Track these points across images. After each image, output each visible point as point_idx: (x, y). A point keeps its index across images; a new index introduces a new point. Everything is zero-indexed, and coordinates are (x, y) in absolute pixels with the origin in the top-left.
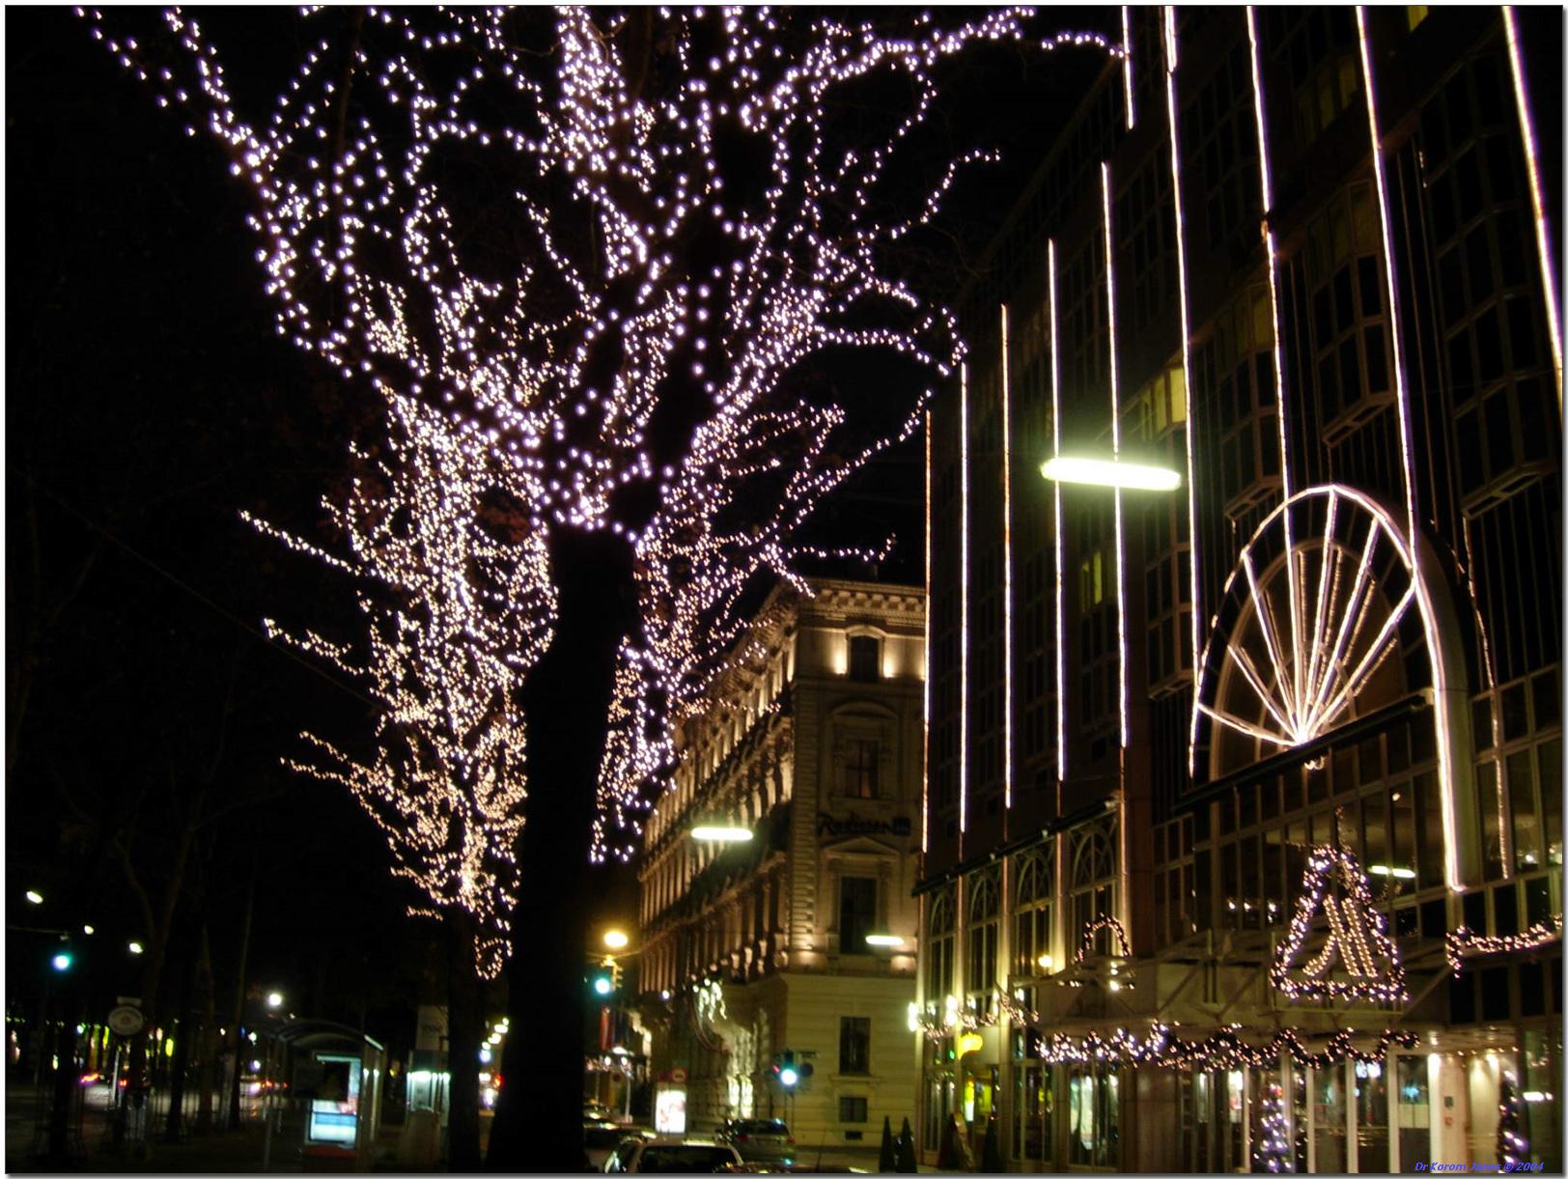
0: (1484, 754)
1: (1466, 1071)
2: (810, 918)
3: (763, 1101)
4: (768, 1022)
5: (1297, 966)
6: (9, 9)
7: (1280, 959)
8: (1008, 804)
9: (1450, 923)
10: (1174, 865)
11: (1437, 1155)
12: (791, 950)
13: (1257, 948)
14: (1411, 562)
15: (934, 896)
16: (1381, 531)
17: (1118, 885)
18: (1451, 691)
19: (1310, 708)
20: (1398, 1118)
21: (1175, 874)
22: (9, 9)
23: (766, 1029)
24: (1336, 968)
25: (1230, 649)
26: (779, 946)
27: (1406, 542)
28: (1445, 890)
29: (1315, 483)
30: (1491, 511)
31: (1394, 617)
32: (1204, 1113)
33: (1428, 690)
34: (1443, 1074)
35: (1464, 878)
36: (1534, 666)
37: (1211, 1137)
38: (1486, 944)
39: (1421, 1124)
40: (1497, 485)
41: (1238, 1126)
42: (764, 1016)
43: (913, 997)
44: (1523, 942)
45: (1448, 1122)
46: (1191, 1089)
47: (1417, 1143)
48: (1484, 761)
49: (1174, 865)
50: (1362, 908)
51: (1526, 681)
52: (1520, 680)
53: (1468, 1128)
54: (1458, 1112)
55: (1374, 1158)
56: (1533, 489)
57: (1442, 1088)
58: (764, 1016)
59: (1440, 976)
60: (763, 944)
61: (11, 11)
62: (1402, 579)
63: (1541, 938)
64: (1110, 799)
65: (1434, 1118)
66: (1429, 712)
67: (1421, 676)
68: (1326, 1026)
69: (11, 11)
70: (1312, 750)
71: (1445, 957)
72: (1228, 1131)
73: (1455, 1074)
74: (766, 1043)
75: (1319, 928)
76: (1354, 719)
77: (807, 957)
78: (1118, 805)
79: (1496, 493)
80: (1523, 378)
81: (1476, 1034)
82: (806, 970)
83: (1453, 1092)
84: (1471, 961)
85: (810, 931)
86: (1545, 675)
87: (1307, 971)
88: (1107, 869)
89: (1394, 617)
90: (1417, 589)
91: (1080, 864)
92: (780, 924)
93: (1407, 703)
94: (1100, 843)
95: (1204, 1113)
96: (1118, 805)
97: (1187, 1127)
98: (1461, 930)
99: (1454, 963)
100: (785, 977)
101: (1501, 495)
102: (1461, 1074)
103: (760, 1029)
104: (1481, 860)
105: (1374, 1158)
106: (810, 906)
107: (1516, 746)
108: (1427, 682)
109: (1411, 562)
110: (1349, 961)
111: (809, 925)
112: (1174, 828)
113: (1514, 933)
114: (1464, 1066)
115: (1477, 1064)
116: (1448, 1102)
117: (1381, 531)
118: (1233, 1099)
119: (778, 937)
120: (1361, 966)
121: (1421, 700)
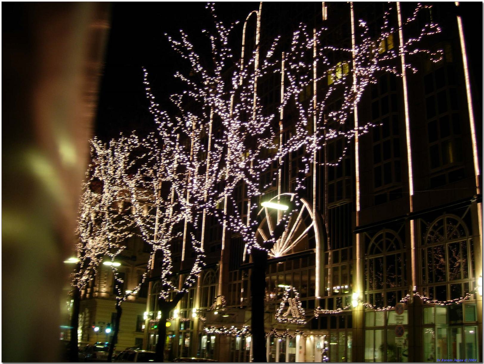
0: (327, 266)
1: (305, 340)
2: (105, 283)
3: (85, 336)
4: (89, 312)
5: (282, 314)
6: (3, 3)
7: (278, 312)
8: (183, 259)
9: (316, 306)
10: (235, 282)
11: (297, 360)
12: (99, 292)
13: (272, 309)
14: (313, 216)
15: (154, 283)
16: (305, 208)
17: (218, 286)
18: (320, 249)
19: (281, 248)
20: (289, 351)
21: (235, 285)
22: (3, 3)
23: (87, 315)
24: (290, 315)
25: (258, 229)
26: (95, 290)
27: (312, 211)
28: (315, 298)
29: (287, 192)
30: (334, 208)
31: (307, 229)
32: (238, 347)
33: (315, 249)
34: (300, 341)
35: (320, 296)
36: (342, 247)
37: (240, 355)
38: (326, 311)
39: (294, 353)
40: (338, 203)
41: (248, 352)
42: (87, 311)
43: (145, 310)
44: (335, 312)
45: (300, 352)
46: (234, 341)
47: (293, 357)
48: (326, 268)
49: (235, 282)
50: (297, 300)
51: (340, 250)
52: (337, 250)
53: (305, 354)
54: (303, 349)
55: (282, 359)
56: (346, 205)
57: (300, 344)
58: (87, 311)
59: (312, 318)
60: (89, 290)
61: (3, 3)
62: (310, 221)
63: (339, 311)
64: (218, 263)
65: (297, 351)
66: (315, 254)
67: (313, 245)
68: (283, 328)
69: (3, 3)
70: (280, 259)
71: (314, 314)
72: (245, 353)
73: (303, 341)
74: (87, 319)
75: (287, 304)
76: (293, 253)
77: (103, 294)
78: (220, 265)
79: (337, 204)
80: (347, 178)
81: (308, 331)
82: (103, 298)
83: (302, 345)
84: (321, 315)
85: (105, 287)
86: (345, 249)
87: (284, 315)
88: (216, 280)
89: (307, 229)
90: (314, 224)
91: (206, 279)
92: (96, 284)
93: (309, 251)
94: (212, 274)
95: (238, 347)
96: (220, 265)
97: (232, 351)
98: (318, 307)
99: (317, 315)
100: (97, 300)
101: (338, 205)
102: (304, 341)
103: (85, 314)
104: (324, 293)
105: (282, 359)
106: (105, 279)
107: (336, 265)
108: (314, 246)
109: (313, 216)
110: (293, 313)
111: (105, 285)
112: (236, 273)
113: (332, 309)
114: (305, 339)
115: (308, 338)
116: (301, 348)
117: (305, 208)
118: (247, 344)
119: (95, 288)
120: (296, 315)
121: (313, 251)
